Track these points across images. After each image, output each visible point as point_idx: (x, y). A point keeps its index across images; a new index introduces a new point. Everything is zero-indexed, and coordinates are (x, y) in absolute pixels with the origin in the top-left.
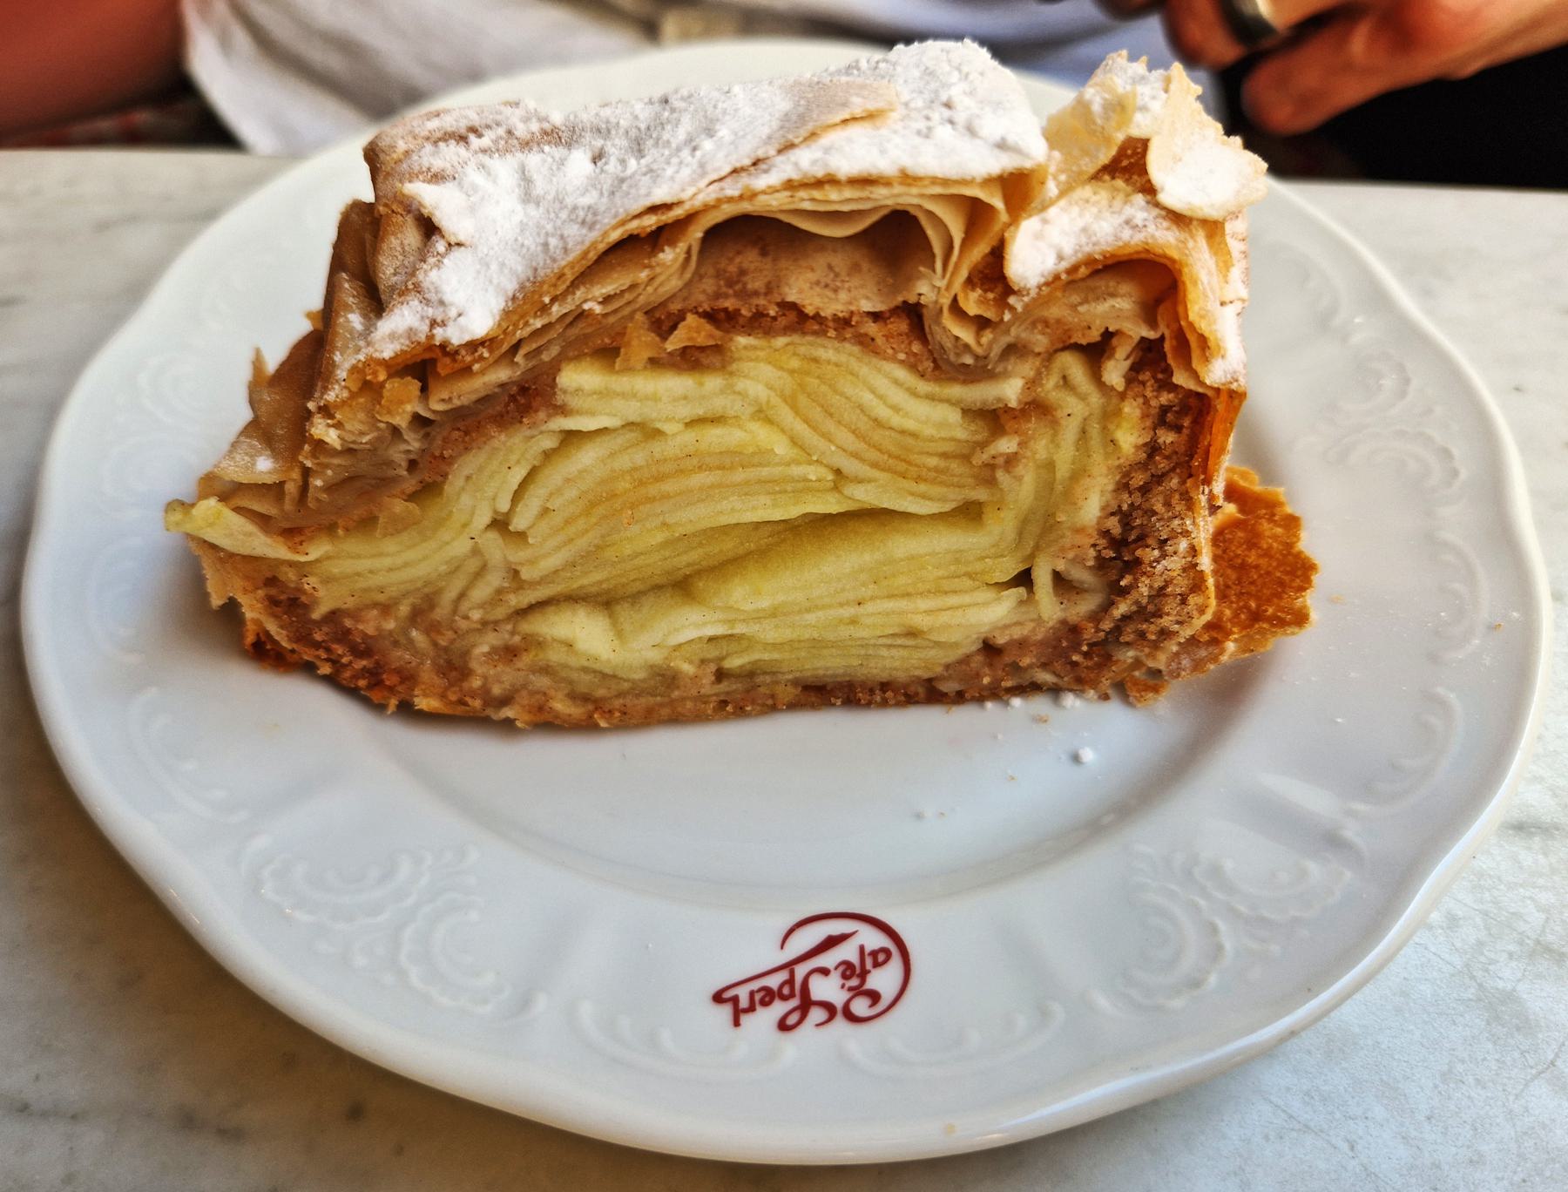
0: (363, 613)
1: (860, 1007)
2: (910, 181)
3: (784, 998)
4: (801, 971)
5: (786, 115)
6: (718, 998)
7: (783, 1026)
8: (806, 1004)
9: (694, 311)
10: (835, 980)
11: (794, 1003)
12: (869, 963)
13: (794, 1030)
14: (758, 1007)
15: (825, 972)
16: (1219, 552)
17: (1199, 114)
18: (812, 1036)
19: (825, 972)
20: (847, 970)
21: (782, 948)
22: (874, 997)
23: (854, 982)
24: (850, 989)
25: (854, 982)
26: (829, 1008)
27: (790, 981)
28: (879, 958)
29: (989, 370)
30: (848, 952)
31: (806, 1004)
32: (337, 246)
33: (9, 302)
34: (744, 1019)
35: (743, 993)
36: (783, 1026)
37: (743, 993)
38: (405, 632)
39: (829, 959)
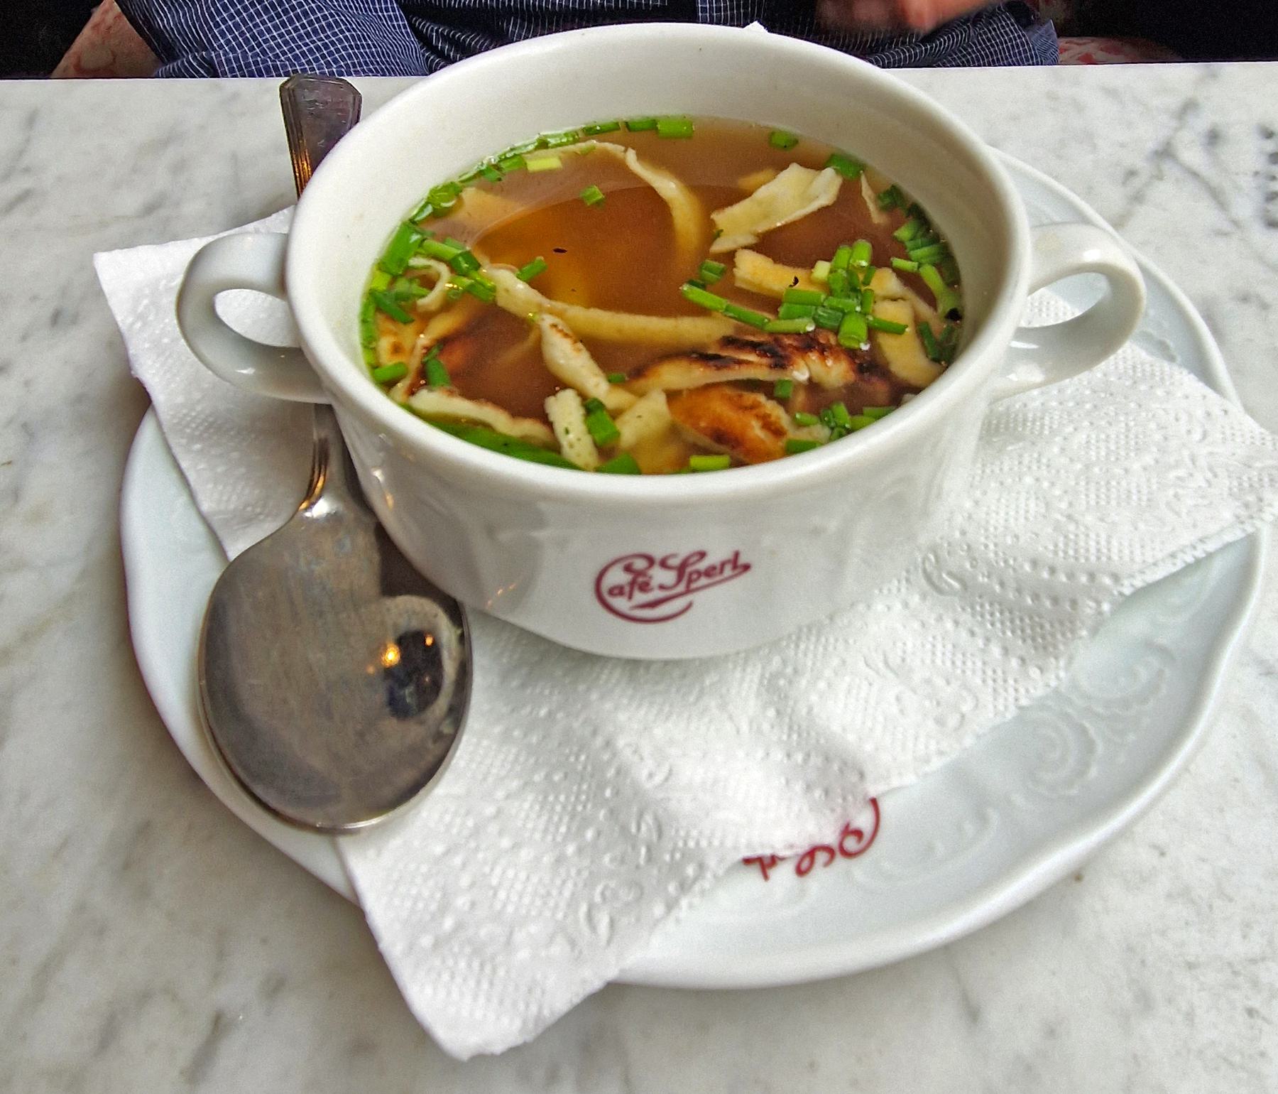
0: (773, 142)
4: (681, 588)
6: (747, 567)
7: (702, 555)
8: (681, 569)
9: (880, 389)
10: (655, 582)
11: (689, 570)
12: (627, 589)
17: (1146, 315)
18: (683, 549)
19: (662, 587)
20: (645, 587)
22: (628, 569)
23: (641, 580)
25: (641, 580)
26: (664, 564)
27: (690, 581)
29: (478, 8)
30: (640, 597)
31: (681, 569)
32: (617, 24)
35: (728, 571)
36: (702, 555)
37: (728, 571)
39: (656, 594)
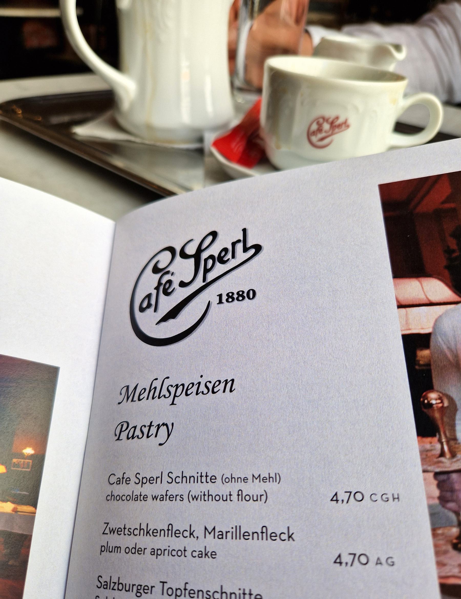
1: (321, 121)
2: (25, 459)
3: (212, 257)
6: (258, 248)
8: (332, 123)
11: (204, 255)
15: (183, 284)
16: (424, 456)
19: (183, 284)
24: (168, 272)
27: (206, 271)
28: (314, 133)
30: (320, 136)
31: (332, 123)
33: (114, 598)
35: (241, 256)
37: (241, 256)
39: (323, 135)
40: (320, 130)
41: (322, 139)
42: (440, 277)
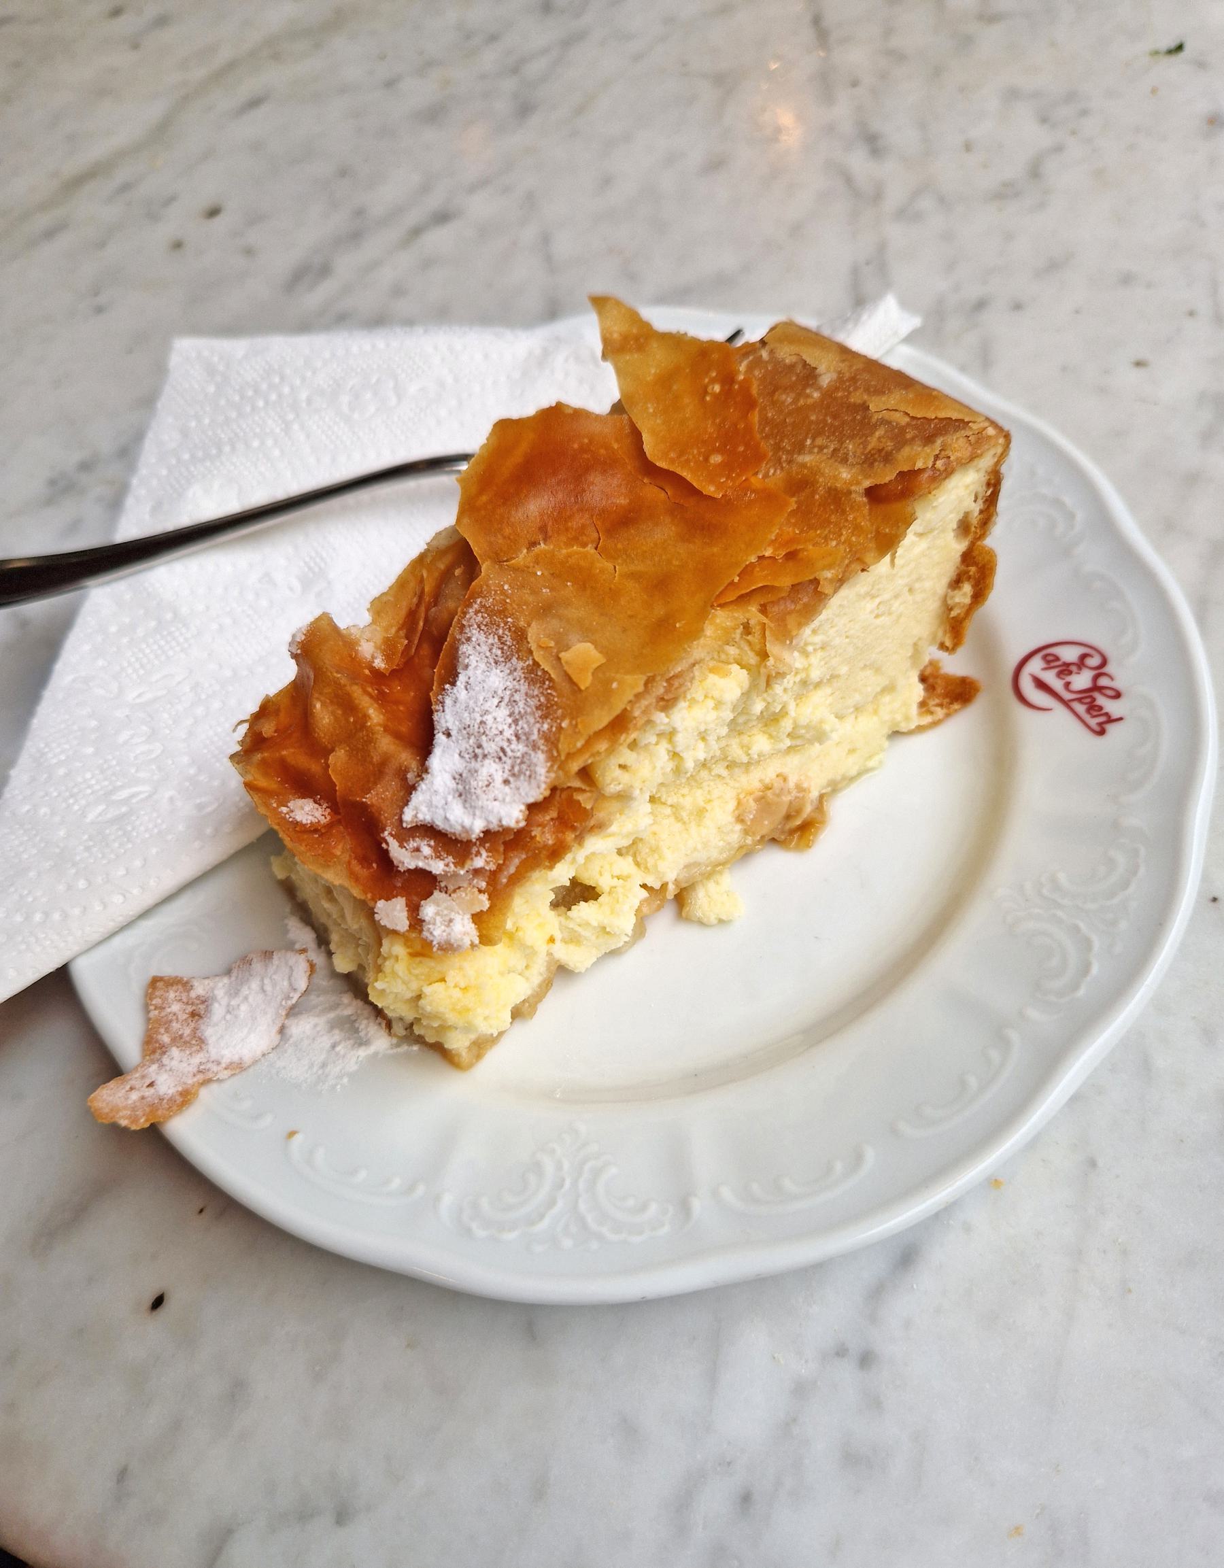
5: (236, 996)
13: (1117, 689)
14: (1104, 711)
15: (1067, 685)
21: (1051, 709)
27: (1080, 700)
28: (1051, 661)
30: (1050, 678)
34: (1115, 715)
35: (1093, 722)
36: (1117, 695)
38: (492, 590)
39: (1057, 684)
40: (1065, 670)
41: (1041, 685)
42: (85, 558)
